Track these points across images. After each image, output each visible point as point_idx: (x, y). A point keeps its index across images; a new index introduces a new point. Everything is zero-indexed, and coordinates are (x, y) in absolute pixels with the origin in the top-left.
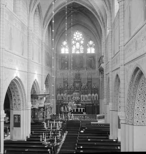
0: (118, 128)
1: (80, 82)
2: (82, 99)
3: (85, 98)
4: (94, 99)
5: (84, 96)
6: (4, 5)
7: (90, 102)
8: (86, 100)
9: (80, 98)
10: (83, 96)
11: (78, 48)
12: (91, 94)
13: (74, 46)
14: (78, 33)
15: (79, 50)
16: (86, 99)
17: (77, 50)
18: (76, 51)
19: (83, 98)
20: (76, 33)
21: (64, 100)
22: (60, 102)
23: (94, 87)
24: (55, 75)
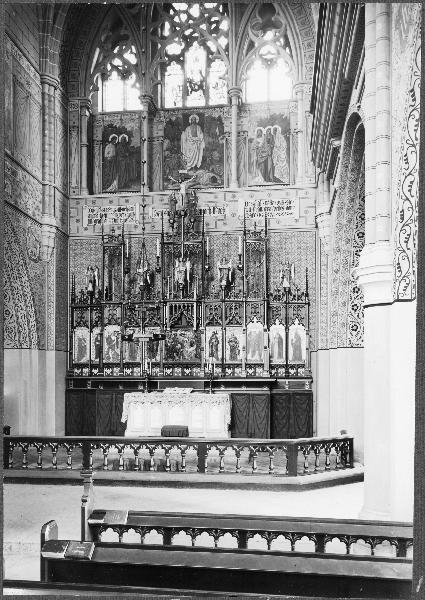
0: (354, 441)
1: (199, 255)
2: (212, 355)
3: (228, 347)
4: (280, 355)
5: (219, 336)
6: (381, 539)
7: (259, 370)
8: (233, 357)
9: (199, 349)
10: (215, 333)
11: (197, 79)
12: (269, 322)
13: (173, 69)
14: (120, 55)
15: (202, 87)
16: (233, 349)
17: (189, 87)
18: (184, 98)
19: (214, 346)
20: (173, 9)
21: (109, 358)
22: (86, 370)
23: (286, 284)
24: (58, 214)
